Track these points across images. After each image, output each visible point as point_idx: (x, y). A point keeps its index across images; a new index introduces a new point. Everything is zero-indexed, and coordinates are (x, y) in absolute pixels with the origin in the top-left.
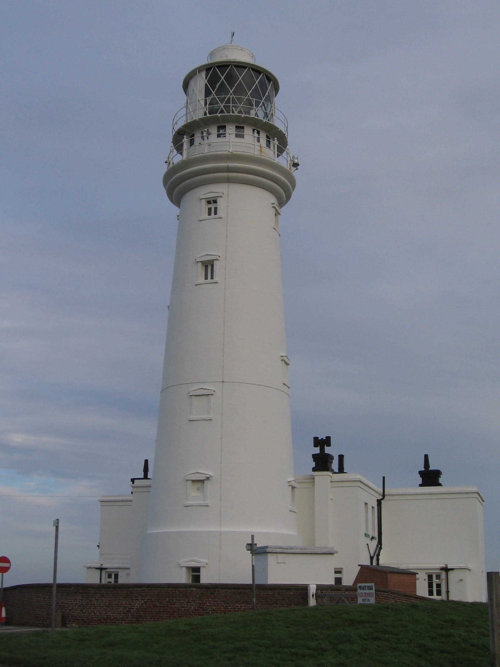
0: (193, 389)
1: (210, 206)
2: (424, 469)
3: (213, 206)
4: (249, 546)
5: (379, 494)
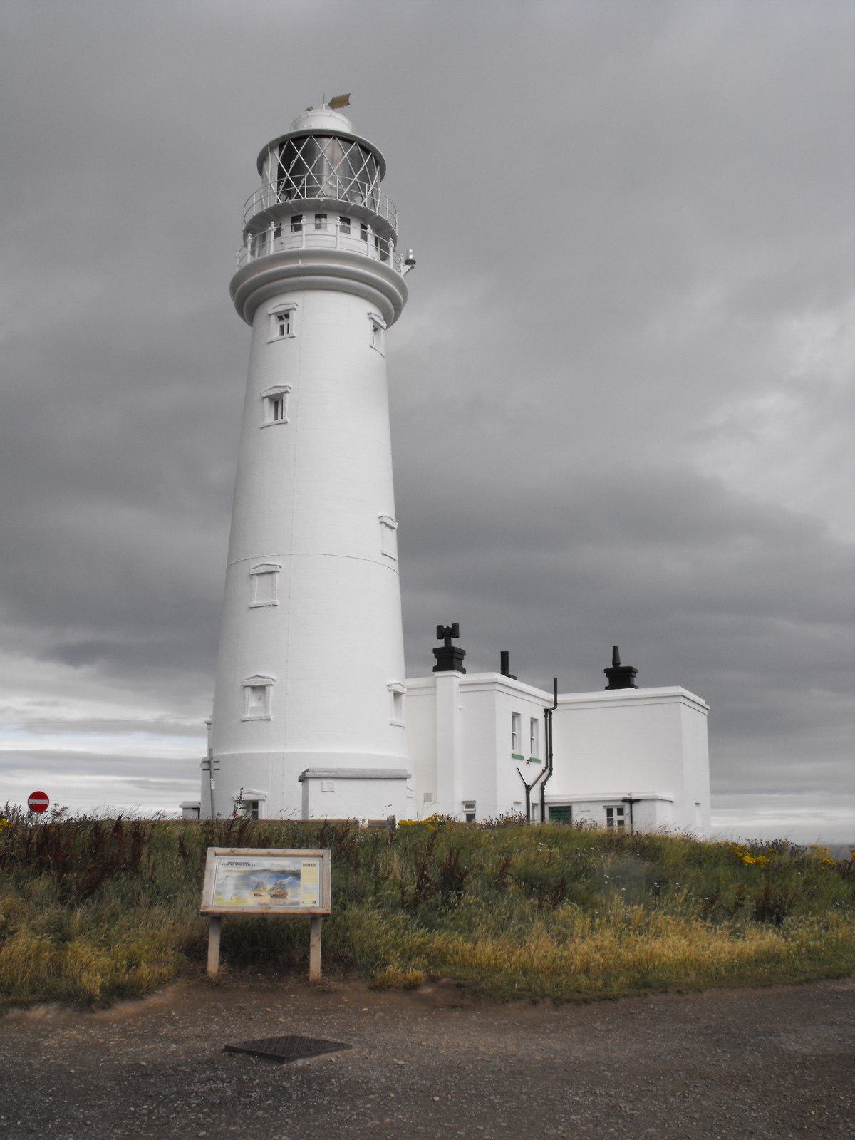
0: (253, 567)
1: (282, 323)
2: (612, 666)
3: (285, 323)
4: (206, 766)
5: (549, 701)
